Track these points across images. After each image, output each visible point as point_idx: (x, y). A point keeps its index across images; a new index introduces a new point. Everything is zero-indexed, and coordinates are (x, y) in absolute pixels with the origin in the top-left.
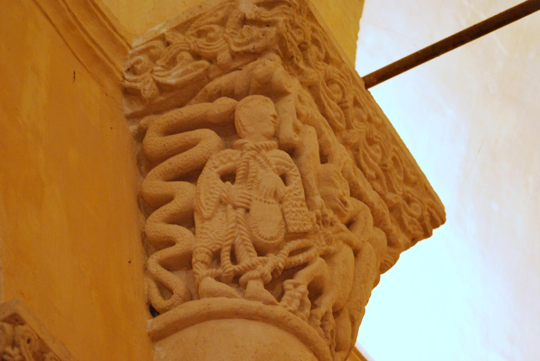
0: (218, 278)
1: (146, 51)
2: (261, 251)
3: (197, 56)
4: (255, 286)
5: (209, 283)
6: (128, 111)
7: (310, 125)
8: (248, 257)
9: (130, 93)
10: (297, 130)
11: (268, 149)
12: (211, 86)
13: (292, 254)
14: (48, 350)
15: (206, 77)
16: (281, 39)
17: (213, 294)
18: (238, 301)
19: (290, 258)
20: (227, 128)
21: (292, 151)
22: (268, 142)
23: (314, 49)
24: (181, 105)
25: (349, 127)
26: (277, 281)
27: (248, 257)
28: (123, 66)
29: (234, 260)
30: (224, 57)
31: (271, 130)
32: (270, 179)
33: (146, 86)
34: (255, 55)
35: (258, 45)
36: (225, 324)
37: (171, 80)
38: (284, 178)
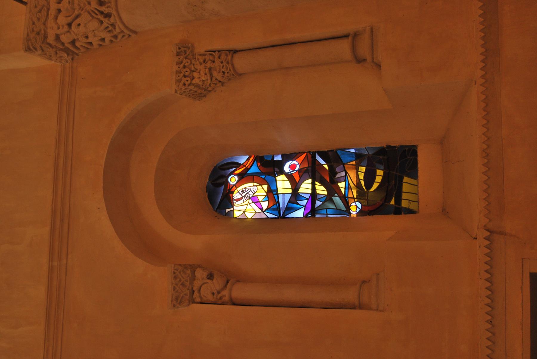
0: (115, 28)
1: (61, 62)
2: (102, 22)
3: (56, 53)
4: (112, 20)
5: (118, 30)
6: (77, 57)
7: (238, 182)
8: (105, 25)
9: (72, 59)
10: (63, 26)
11: (74, 32)
12: (61, 47)
13: (97, 15)
14: (176, 71)
15: (61, 50)
16: (43, 43)
17: (119, 27)
18: (119, 23)
19: (528, 275)
20: (73, 43)
21: (70, 25)
22: (72, 33)
23: (35, 30)
24: (68, 48)
25: (44, 6)
26: (108, 16)
27: (105, 25)
28: (67, 65)
29: (107, 28)
30: (54, 50)
31: (68, 34)
32: (82, 29)
33: (70, 58)
34: (49, 44)
35: (48, 46)
36: (126, 23)
37: (66, 55)
38: (79, 25)
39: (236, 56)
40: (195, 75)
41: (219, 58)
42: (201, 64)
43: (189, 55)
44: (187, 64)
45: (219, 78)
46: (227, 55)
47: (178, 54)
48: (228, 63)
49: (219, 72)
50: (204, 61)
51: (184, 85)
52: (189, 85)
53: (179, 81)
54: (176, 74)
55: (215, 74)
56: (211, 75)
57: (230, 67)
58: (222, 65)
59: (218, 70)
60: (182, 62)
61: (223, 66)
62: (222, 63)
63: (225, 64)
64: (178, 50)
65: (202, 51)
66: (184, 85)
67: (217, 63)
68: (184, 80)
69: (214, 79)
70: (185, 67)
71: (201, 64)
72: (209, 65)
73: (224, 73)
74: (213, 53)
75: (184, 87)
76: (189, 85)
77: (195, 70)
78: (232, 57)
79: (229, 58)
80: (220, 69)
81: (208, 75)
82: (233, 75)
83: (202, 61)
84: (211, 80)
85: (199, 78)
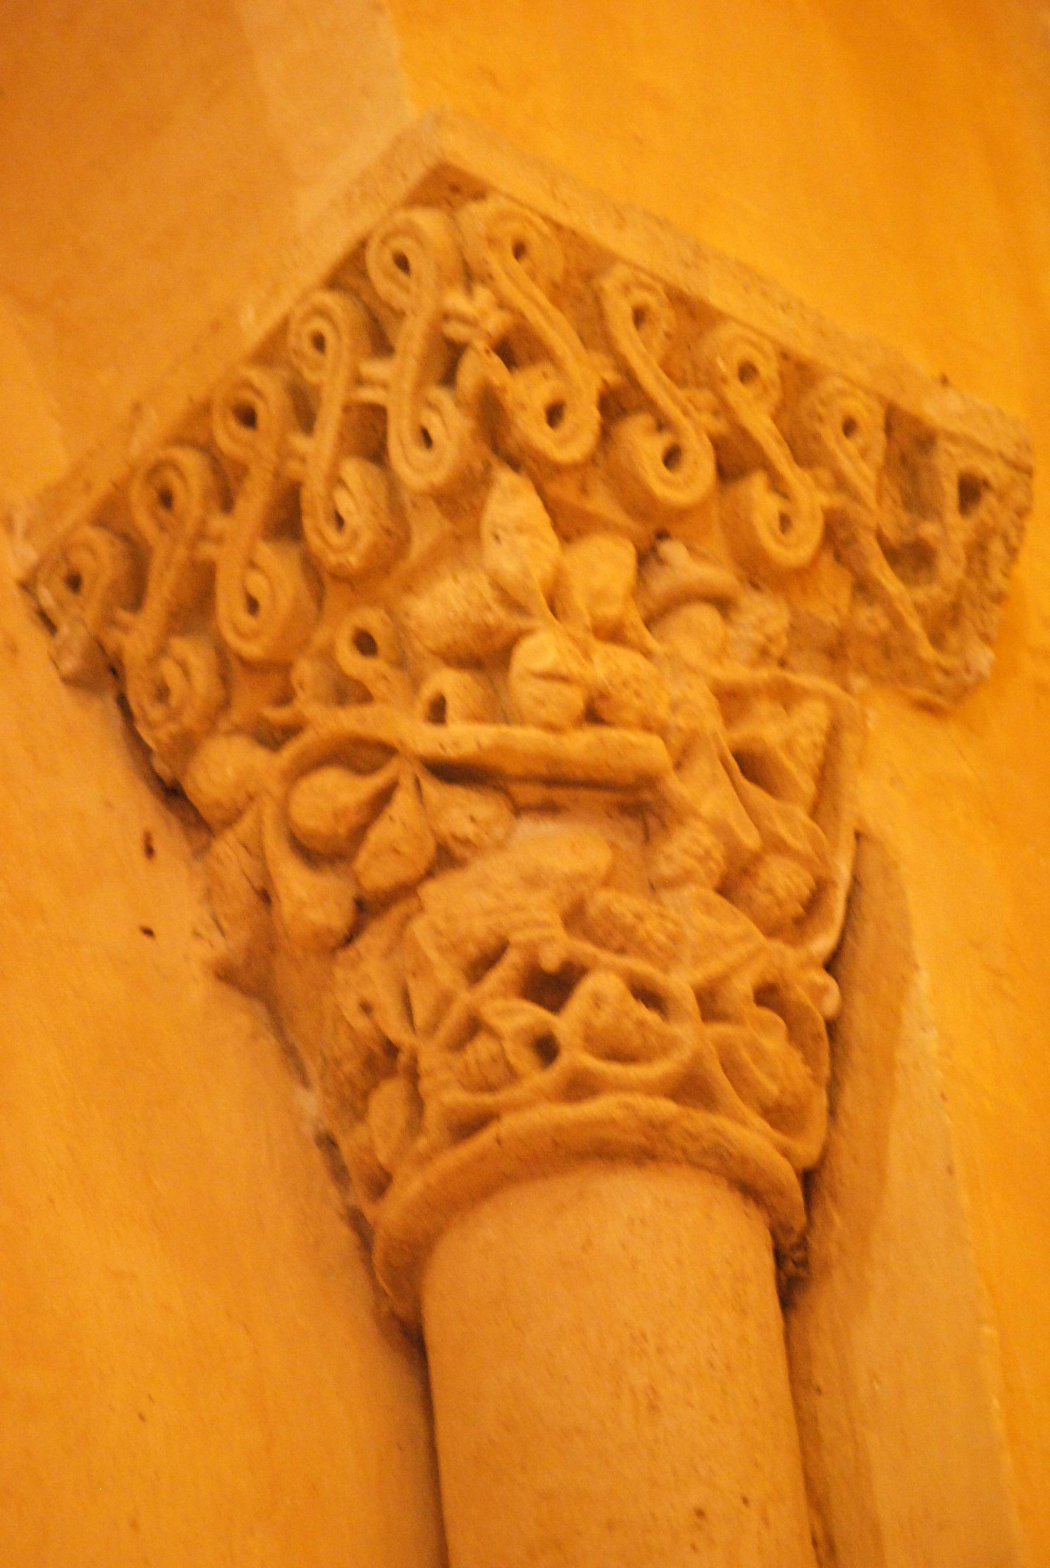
38: (402, 262)
39: (736, 1244)
40: (604, 566)
41: (767, 995)
42: (732, 700)
43: (864, 588)
44: (760, 500)
45: (459, 907)
46: (780, 1116)
47: (910, 444)
48: (691, 1088)
49: (575, 917)
50: (752, 766)
51: (515, 349)
52: (491, 415)
53: (579, 285)
54: (678, 299)
55: (570, 849)
56: (552, 790)
57: (627, 1100)
58: (680, 983)
59: (626, 905)
60: (806, 452)
61: (649, 995)
62: (710, 1003)
63: (689, 1036)
64: (948, 465)
65: (871, 796)
66: (515, 349)
67: (707, 940)
68: (584, 377)
69: (463, 812)
70: (734, 460)
71: (732, 700)
72: (707, 795)
73: (551, 987)
74: (823, 943)
75: (495, 322)
76: (491, 415)
77: (661, 584)
78: (750, 1189)
79: (754, 1138)
80: (619, 938)
81: (580, 745)
82: (467, 1126)
83: (766, 728)
84: (450, 772)
85: (556, 603)
